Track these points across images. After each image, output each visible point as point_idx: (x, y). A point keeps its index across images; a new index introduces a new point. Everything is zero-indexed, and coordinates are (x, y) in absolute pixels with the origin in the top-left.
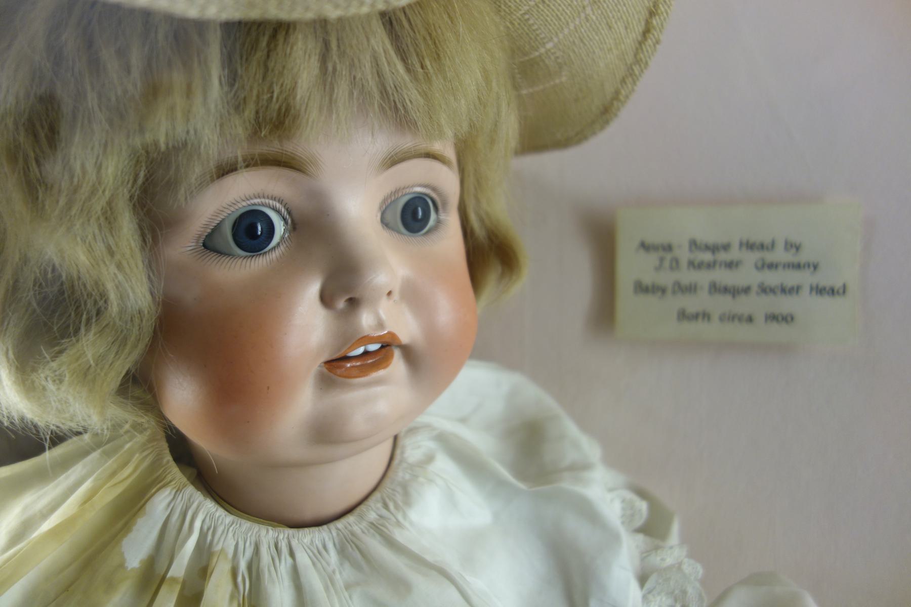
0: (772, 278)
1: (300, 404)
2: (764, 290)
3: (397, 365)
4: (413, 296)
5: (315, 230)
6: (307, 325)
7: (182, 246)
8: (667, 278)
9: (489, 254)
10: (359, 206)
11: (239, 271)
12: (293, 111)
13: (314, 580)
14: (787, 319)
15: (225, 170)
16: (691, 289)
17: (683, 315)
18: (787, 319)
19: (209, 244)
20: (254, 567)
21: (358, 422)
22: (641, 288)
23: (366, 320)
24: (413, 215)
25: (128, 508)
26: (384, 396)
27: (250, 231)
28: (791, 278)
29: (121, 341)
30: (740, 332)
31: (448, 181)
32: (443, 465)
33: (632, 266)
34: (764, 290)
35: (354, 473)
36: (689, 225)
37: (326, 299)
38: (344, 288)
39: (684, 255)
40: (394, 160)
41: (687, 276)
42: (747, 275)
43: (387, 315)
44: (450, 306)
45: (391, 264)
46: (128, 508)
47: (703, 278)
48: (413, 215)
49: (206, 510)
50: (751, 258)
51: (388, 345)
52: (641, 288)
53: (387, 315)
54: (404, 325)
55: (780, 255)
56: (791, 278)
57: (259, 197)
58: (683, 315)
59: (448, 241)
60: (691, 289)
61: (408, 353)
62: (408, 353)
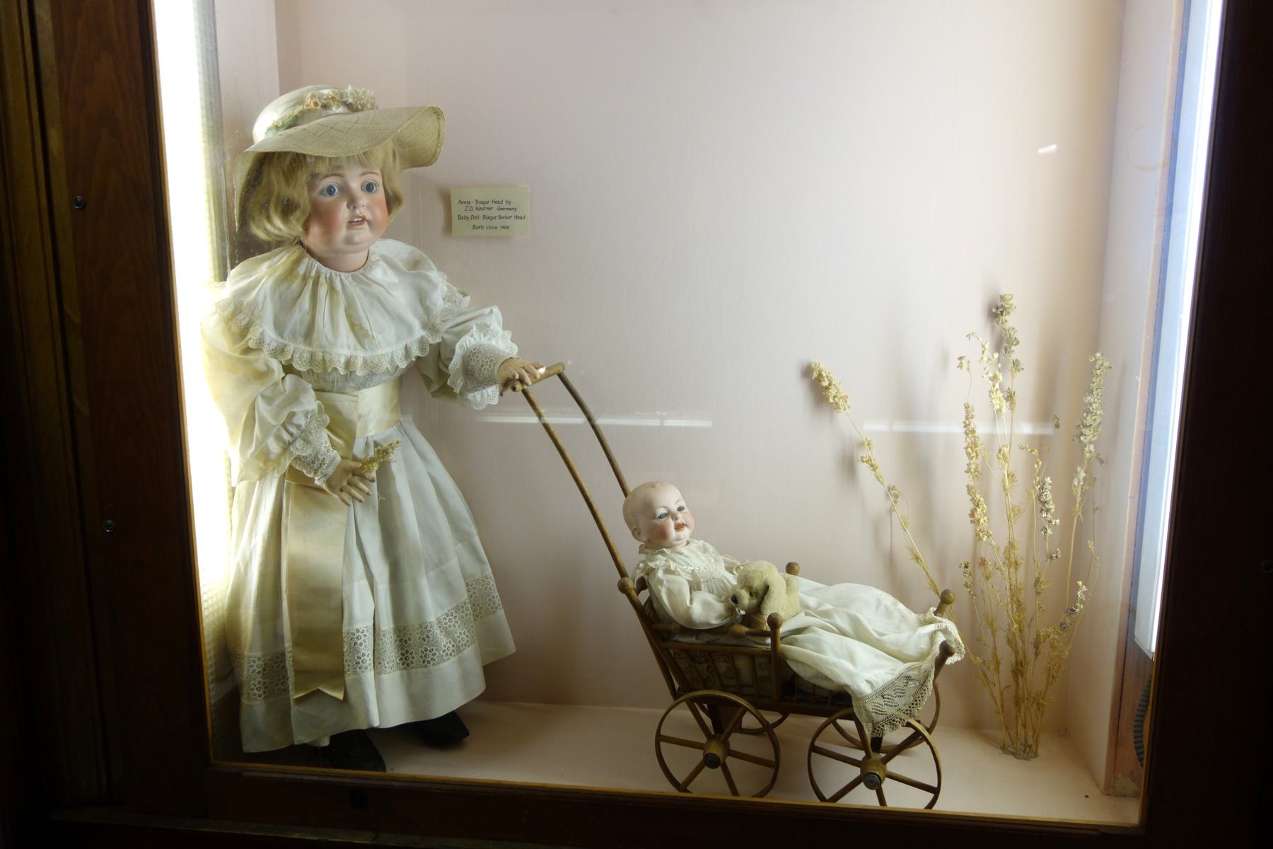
0: (503, 213)
1: (342, 233)
2: (500, 218)
3: (366, 225)
4: (369, 208)
5: (346, 191)
6: (344, 213)
7: (316, 194)
8: (469, 214)
9: (392, 201)
10: (355, 185)
11: (328, 199)
12: (235, 329)
13: (346, 282)
14: (507, 228)
15: (327, 176)
16: (477, 217)
17: (474, 227)
18: (507, 228)
19: (321, 193)
20: (331, 278)
21: (357, 239)
22: (460, 217)
23: (358, 212)
24: (369, 188)
25: (297, 262)
26: (363, 233)
27: (330, 191)
28: (508, 213)
29: (304, 212)
30: (492, 232)
31: (379, 179)
32: (382, 262)
33: (457, 210)
34: (500, 218)
35: (358, 259)
36: (474, 195)
37: (348, 206)
38: (352, 203)
39: (474, 205)
40: (364, 174)
41: (476, 213)
42: (494, 213)
43: (362, 211)
44: (380, 212)
45: (363, 199)
46: (297, 262)
47: (481, 213)
48: (369, 188)
49: (317, 264)
50: (496, 206)
51: (364, 219)
52: (460, 217)
53: (362, 211)
54: (368, 216)
55: (504, 205)
56: (508, 213)
57: (1142, 721)
58: (474, 227)
59: (380, 194)
60: (477, 217)
61: (369, 222)
62: (369, 222)
